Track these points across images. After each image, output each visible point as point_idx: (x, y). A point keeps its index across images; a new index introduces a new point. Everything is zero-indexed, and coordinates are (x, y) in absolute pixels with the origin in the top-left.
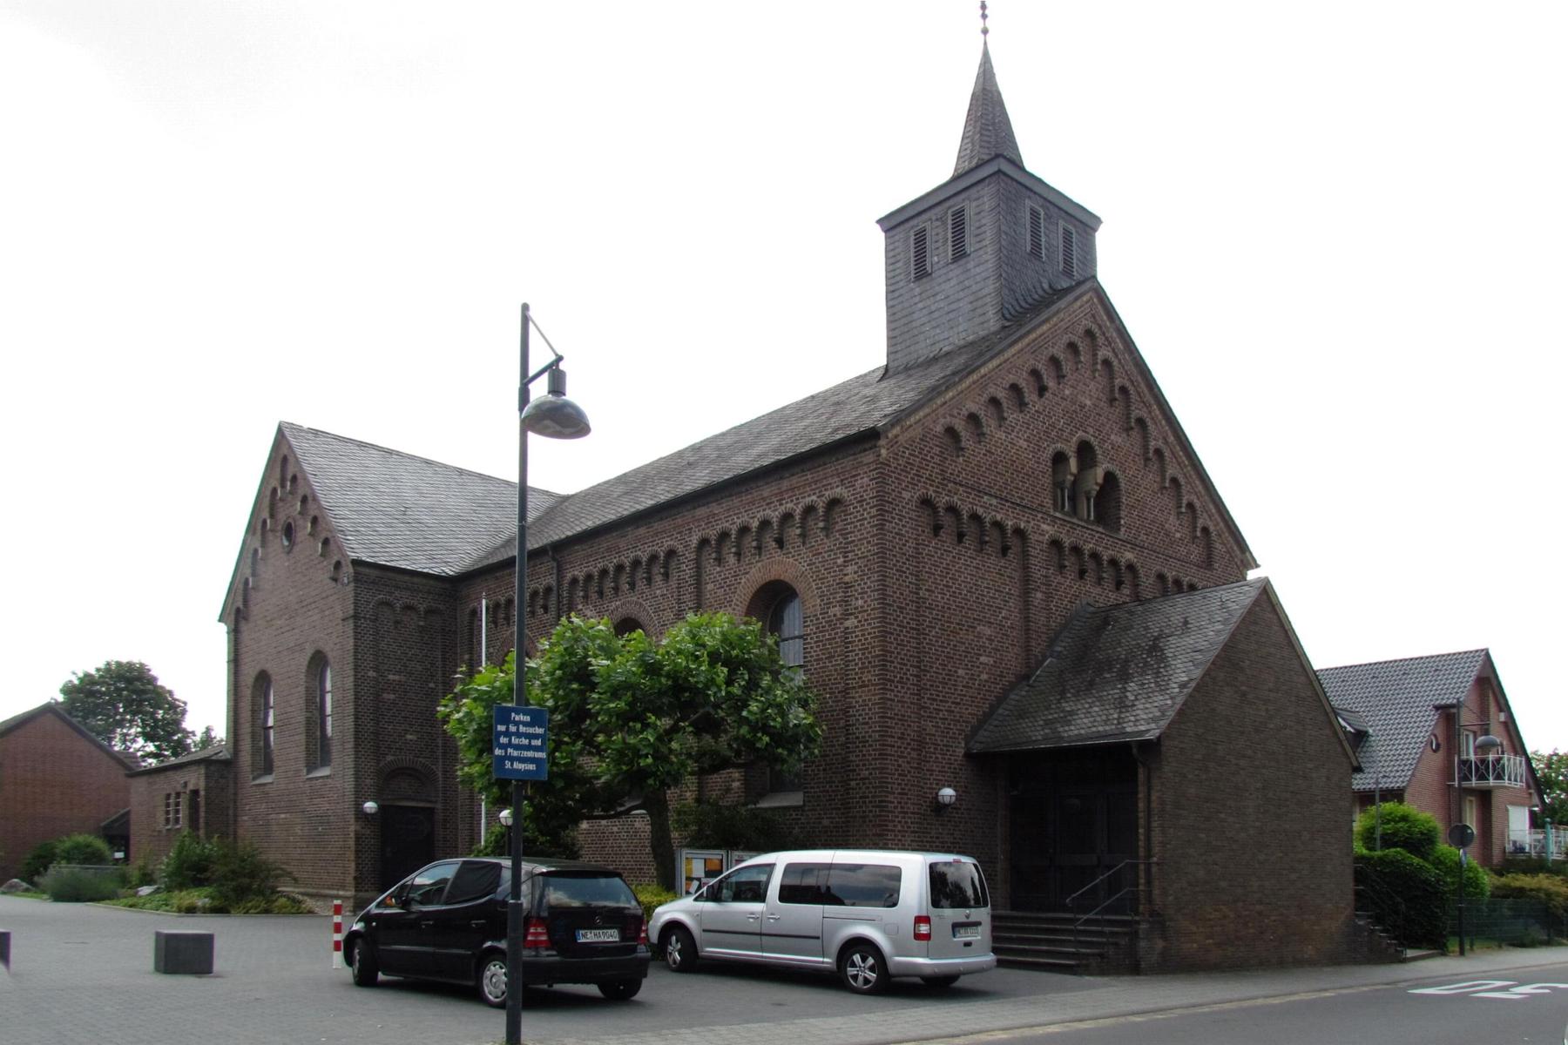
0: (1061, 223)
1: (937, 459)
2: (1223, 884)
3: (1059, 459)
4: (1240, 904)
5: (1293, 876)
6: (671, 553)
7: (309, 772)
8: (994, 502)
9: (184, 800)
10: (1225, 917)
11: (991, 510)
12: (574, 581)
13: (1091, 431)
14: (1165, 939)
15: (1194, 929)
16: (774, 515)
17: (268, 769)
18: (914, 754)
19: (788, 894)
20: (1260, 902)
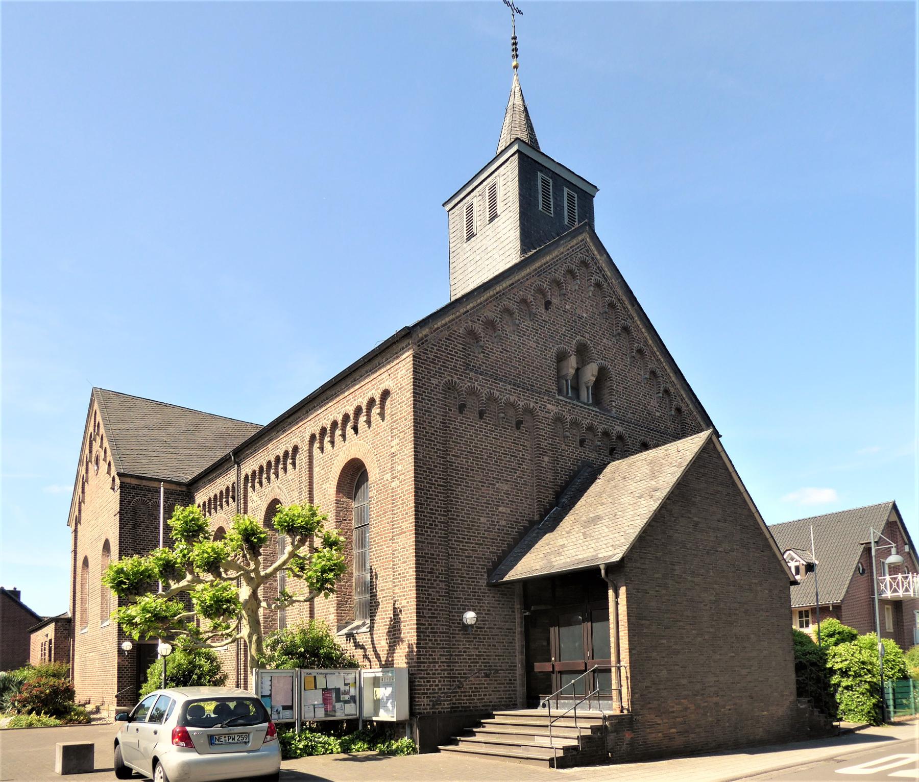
0: (566, 190)
1: (460, 354)
2: (684, 681)
3: (561, 357)
4: (699, 697)
5: (744, 672)
7: (102, 623)
8: (509, 387)
9: (47, 644)
10: (686, 709)
11: (506, 394)
13: (587, 336)
14: (633, 731)
15: (659, 721)
16: (351, 410)
18: (442, 585)
20: (717, 694)
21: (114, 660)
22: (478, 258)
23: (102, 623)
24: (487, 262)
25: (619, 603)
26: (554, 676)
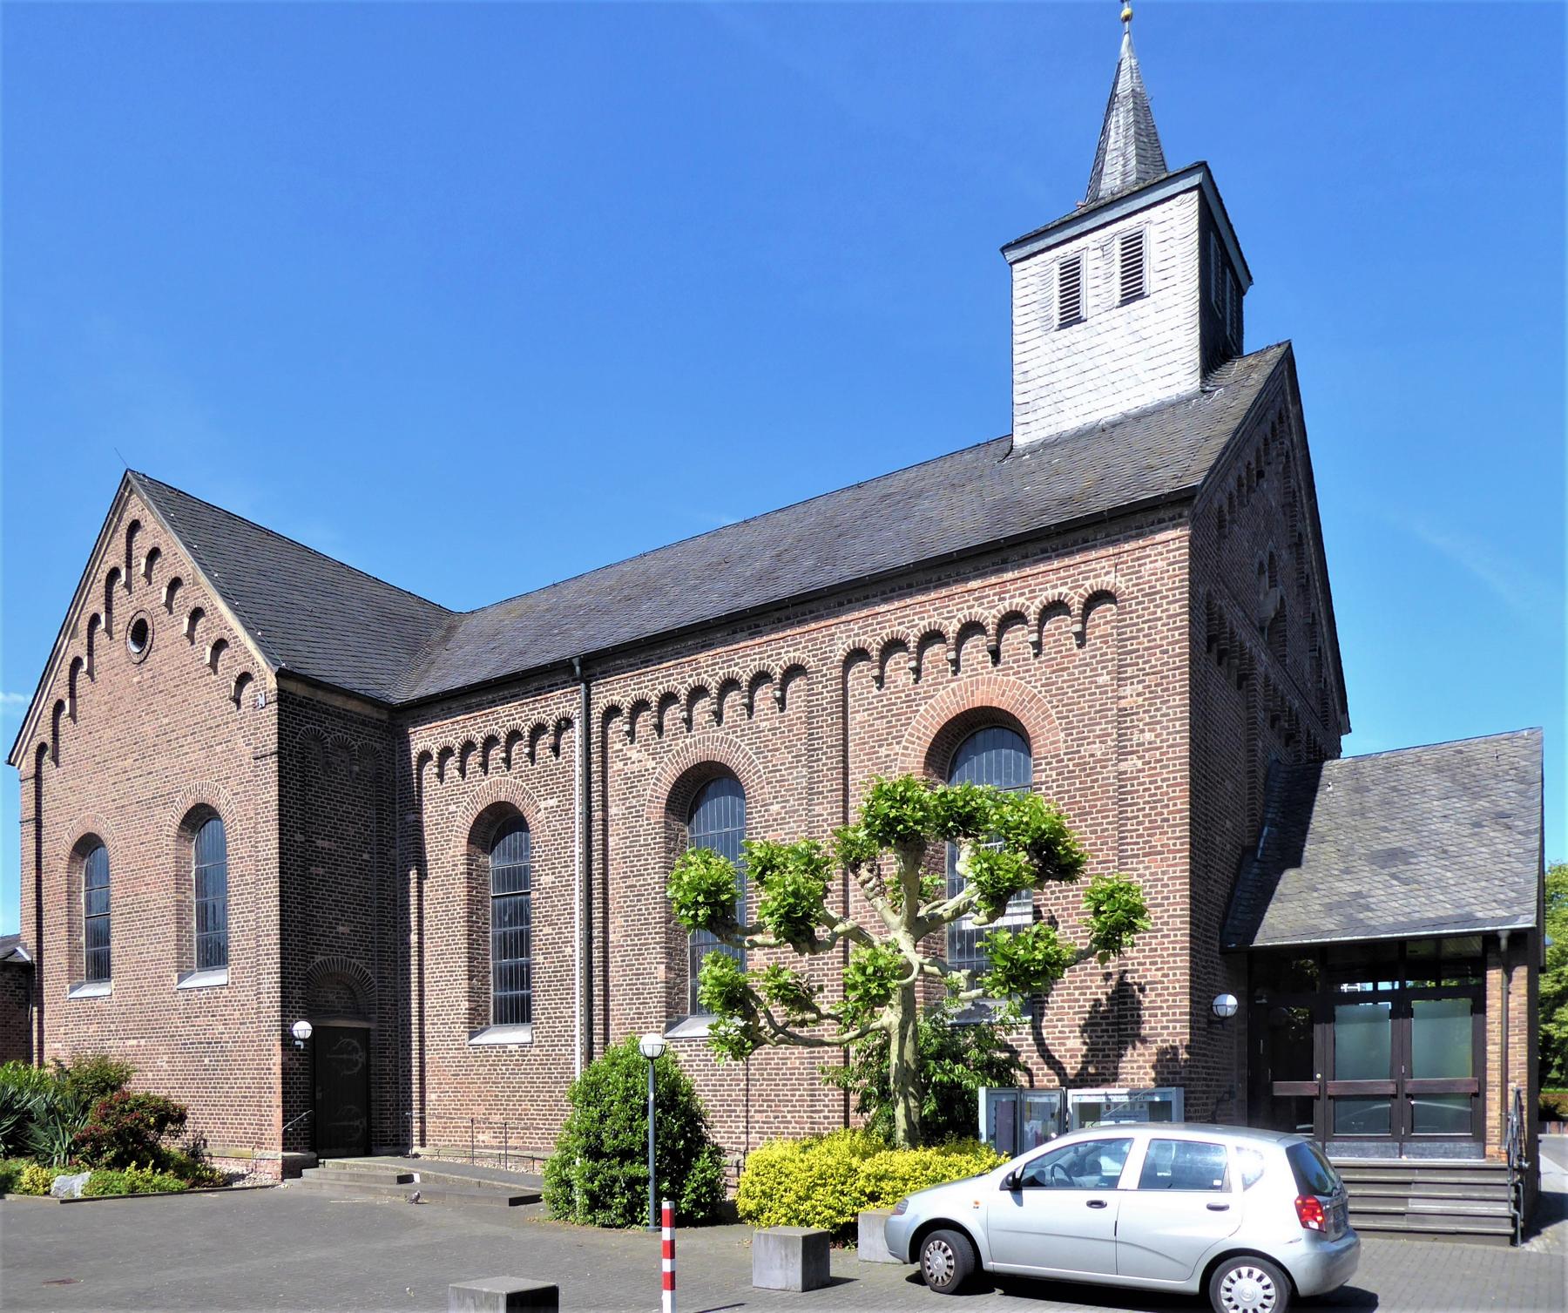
6: (795, 671)
7: (180, 979)
12: (612, 711)
17: (100, 969)
19: (1149, 1180)
21: (276, 1060)
22: (1089, 365)
23: (180, 979)
24: (1113, 377)
25: (1507, 994)
26: (1318, 1105)
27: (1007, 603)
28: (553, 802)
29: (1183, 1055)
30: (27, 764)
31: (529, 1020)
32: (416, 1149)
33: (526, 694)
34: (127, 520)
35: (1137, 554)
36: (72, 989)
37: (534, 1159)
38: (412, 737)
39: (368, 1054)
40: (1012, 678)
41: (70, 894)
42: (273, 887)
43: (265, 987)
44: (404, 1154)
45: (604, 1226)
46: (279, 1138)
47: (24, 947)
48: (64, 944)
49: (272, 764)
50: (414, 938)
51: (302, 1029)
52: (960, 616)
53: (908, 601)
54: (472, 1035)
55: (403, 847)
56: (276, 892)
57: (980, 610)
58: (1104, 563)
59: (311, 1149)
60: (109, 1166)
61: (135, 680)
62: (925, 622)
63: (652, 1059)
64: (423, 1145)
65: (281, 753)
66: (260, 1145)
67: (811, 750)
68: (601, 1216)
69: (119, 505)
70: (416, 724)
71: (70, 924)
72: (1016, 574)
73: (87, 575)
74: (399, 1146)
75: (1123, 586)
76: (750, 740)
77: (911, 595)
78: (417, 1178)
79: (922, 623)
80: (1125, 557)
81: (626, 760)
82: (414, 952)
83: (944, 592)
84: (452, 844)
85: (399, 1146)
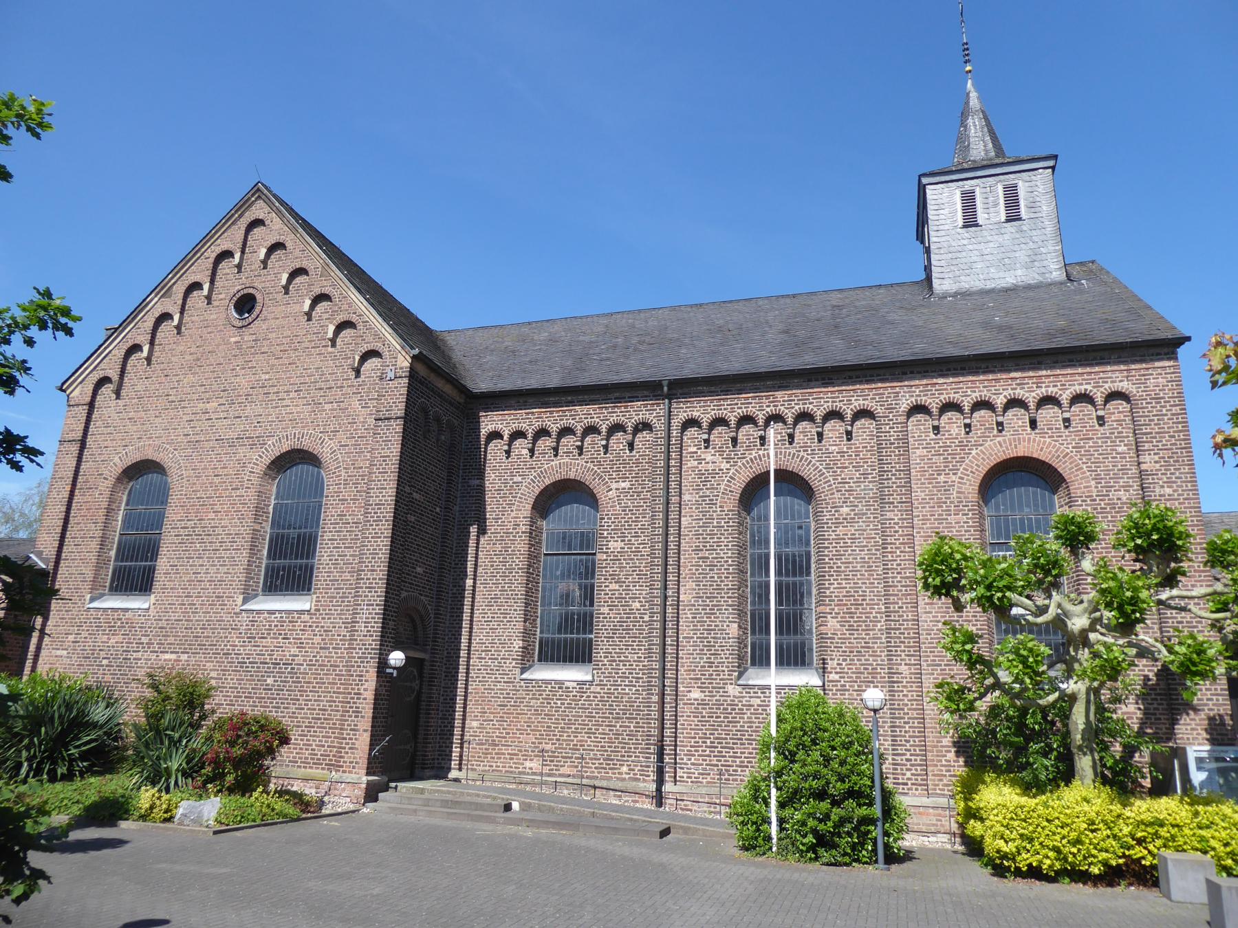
7: (245, 601)
12: (691, 423)
27: (1043, 390)
28: (626, 485)
29: (1228, 721)
30: (81, 393)
31: (590, 661)
32: (453, 774)
33: (606, 401)
34: (249, 216)
35: (1142, 372)
36: (92, 600)
37: (595, 787)
38: (482, 419)
39: (421, 682)
40: (1048, 440)
41: (109, 510)
42: (386, 529)
43: (361, 618)
44: (444, 777)
45: (827, 864)
46: (363, 763)
47: (39, 554)
48: (93, 557)
49: (397, 426)
50: (469, 582)
51: (397, 658)
52: (942, 397)
53: (961, 379)
54: (523, 671)
55: (472, 510)
56: (388, 533)
57: (1022, 392)
58: (1117, 374)
59: (382, 773)
60: (231, 790)
61: (233, 340)
62: (977, 394)
63: (875, 711)
64: (460, 769)
65: (408, 418)
66: (337, 767)
67: (882, 472)
68: (825, 855)
69: (243, 205)
70: (487, 409)
71: (104, 539)
72: (1049, 372)
73: (196, 250)
74: (440, 772)
75: (1134, 391)
76: (825, 458)
77: (963, 375)
78: (515, 806)
79: (974, 395)
80: (1133, 373)
81: (700, 460)
82: (468, 594)
83: (991, 377)
84: (514, 508)
85: (440, 772)
